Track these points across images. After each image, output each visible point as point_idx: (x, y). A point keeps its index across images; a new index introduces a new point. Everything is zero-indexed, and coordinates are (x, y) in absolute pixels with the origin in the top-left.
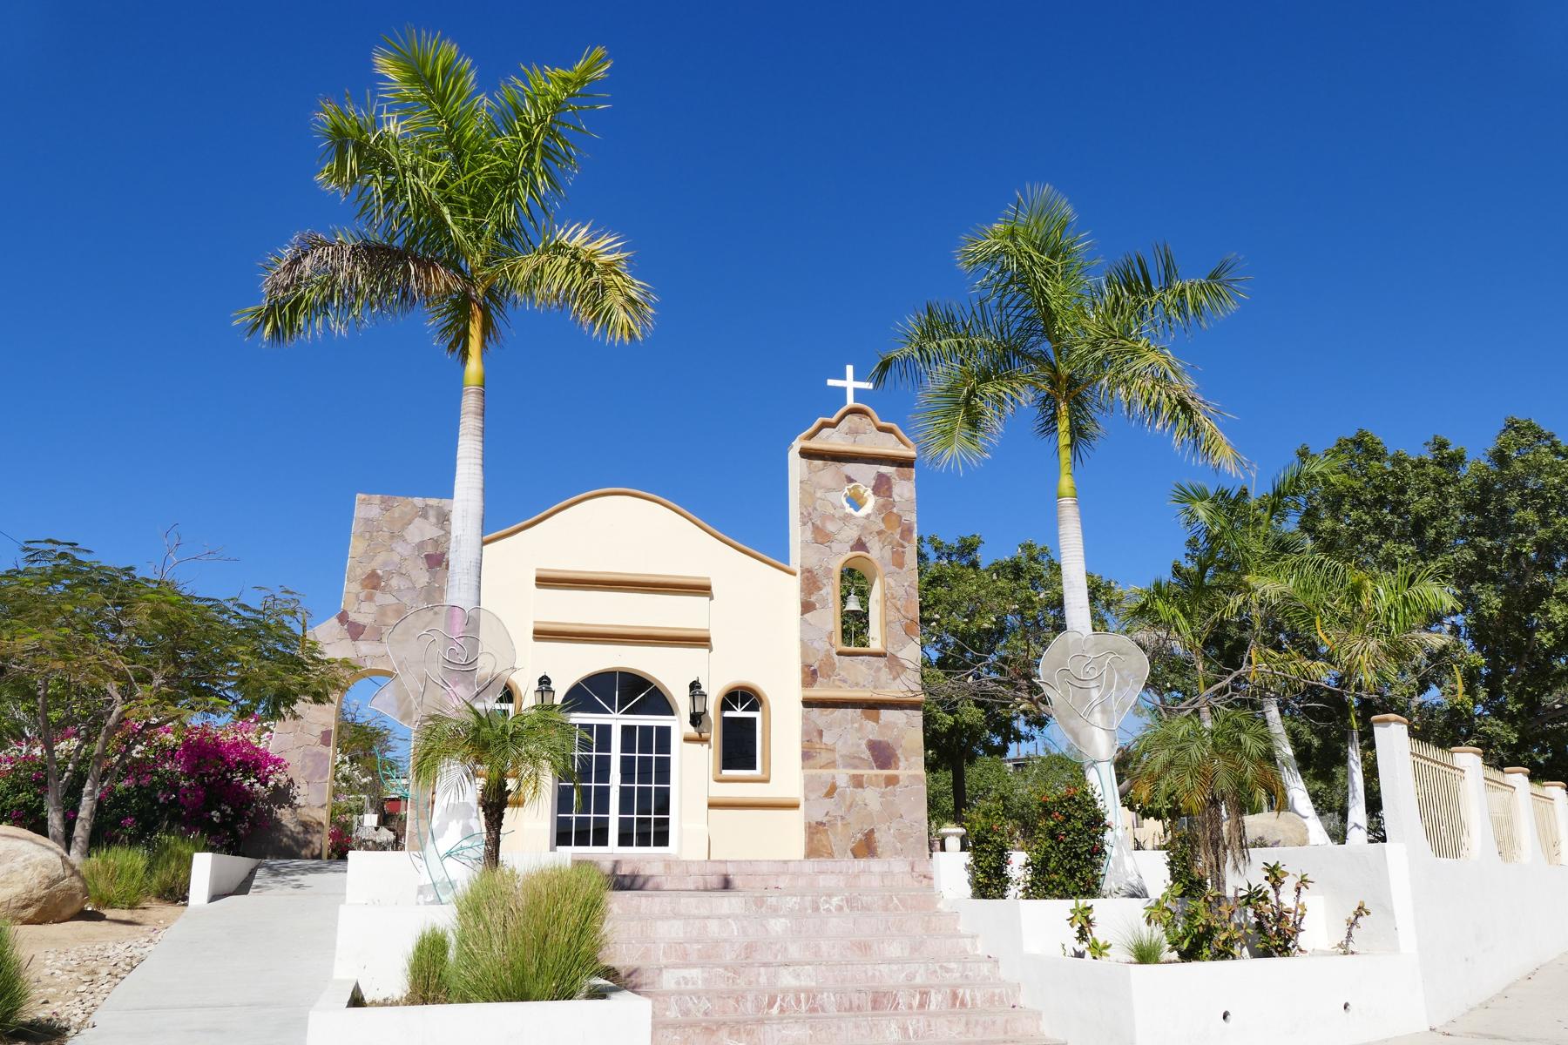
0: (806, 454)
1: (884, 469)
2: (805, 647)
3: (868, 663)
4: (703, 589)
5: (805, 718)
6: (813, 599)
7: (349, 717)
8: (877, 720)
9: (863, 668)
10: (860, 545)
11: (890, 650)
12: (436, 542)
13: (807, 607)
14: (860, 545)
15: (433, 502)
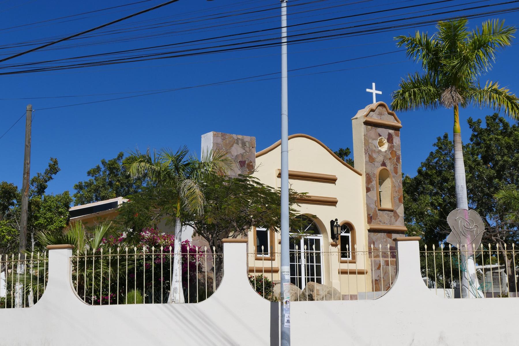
0: (367, 123)
1: (391, 131)
2: (368, 208)
3: (388, 214)
4: (332, 180)
5: (369, 236)
6: (370, 186)
7: (511, 211)
8: (391, 238)
9: (386, 216)
10: (384, 164)
11: (395, 209)
12: (242, 155)
13: (368, 190)
14: (384, 164)
15: (240, 137)
